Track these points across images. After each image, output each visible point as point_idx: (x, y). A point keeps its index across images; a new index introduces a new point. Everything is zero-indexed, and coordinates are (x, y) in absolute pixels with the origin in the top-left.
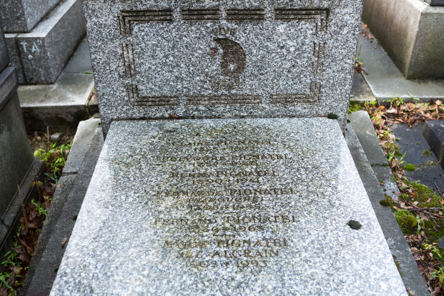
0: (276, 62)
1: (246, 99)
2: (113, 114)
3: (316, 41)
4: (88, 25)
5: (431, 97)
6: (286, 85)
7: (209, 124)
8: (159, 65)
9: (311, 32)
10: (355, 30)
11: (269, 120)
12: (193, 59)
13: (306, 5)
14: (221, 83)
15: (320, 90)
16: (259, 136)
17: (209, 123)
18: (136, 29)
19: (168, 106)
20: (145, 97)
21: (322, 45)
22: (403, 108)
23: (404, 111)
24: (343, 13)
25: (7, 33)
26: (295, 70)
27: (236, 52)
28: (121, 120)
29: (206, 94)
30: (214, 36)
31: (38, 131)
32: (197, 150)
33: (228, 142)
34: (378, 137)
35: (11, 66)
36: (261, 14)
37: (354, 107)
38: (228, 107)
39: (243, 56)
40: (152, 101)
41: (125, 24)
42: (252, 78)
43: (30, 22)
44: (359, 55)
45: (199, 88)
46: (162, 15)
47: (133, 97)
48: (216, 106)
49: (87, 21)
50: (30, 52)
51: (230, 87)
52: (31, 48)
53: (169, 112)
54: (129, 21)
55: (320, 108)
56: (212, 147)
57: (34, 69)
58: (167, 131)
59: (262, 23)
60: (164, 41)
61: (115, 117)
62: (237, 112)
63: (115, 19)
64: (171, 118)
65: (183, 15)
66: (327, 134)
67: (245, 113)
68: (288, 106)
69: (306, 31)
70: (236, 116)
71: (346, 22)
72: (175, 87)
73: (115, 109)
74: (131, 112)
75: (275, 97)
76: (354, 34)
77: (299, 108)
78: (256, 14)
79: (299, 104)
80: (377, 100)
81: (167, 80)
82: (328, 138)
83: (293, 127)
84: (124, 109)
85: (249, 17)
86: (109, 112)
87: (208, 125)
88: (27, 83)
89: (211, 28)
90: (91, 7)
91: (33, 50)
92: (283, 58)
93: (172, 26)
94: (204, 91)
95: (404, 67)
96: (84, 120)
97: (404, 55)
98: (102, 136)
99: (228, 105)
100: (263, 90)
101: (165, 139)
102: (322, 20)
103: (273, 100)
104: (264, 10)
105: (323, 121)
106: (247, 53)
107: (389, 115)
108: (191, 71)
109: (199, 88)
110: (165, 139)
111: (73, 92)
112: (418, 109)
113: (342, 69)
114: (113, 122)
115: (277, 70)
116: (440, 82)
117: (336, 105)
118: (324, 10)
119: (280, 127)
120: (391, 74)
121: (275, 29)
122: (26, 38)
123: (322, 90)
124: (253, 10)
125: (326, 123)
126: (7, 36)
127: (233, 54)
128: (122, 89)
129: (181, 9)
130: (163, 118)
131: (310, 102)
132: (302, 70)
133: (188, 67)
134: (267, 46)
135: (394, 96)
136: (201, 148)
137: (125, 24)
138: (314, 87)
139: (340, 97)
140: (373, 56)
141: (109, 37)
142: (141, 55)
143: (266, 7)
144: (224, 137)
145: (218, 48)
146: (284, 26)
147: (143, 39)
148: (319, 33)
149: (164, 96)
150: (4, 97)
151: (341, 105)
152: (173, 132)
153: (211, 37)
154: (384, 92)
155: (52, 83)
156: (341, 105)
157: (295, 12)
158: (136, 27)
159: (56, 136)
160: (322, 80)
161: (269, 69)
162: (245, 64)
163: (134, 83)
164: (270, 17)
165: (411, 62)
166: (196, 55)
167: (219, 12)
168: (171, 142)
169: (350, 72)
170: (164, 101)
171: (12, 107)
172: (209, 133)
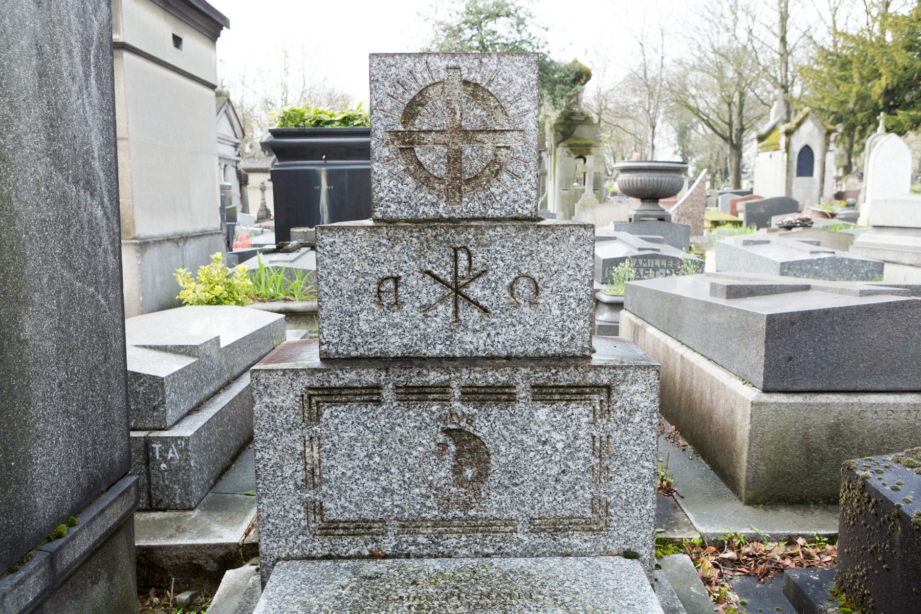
0: (536, 466)
1: (492, 525)
2: (281, 549)
3: (595, 433)
4: (257, 407)
5: (787, 532)
6: (554, 503)
7: (434, 566)
8: (357, 469)
9: (586, 419)
10: (651, 417)
11: (530, 561)
12: (410, 460)
13: (577, 380)
14: (453, 499)
15: (607, 511)
16: (513, 585)
17: (432, 565)
18: (326, 414)
19: (369, 537)
20: (333, 522)
21: (604, 439)
22: (745, 550)
23: (748, 555)
24: (631, 392)
25: (134, 429)
26: (566, 478)
27: (475, 450)
28: (293, 559)
29: (429, 516)
30: (442, 425)
31: (157, 588)
32: (413, 609)
33: (463, 595)
34: (712, 598)
35: (131, 475)
36: (511, 393)
37: (667, 549)
38: (464, 538)
39: (486, 456)
40: (344, 528)
41: (310, 407)
42: (501, 491)
43: (171, 415)
44: (666, 468)
45: (418, 507)
46: (366, 394)
47: (314, 522)
48: (445, 537)
49: (254, 402)
50: (165, 459)
51: (467, 506)
52: (168, 453)
53: (369, 547)
54: (318, 402)
55: (611, 541)
56: (436, 603)
57: (166, 486)
58: (365, 577)
59: (513, 406)
60: (367, 432)
61: (283, 555)
62: (478, 548)
63: (297, 399)
64: (373, 556)
65: (397, 393)
66: (625, 583)
67: (491, 548)
68: (559, 538)
69: (578, 419)
70: (476, 553)
71: (637, 405)
72: (381, 505)
73: (284, 540)
74: (309, 545)
75: (538, 521)
76: (651, 423)
77: (576, 540)
78: (505, 393)
79: (576, 534)
80: (701, 537)
81: (370, 494)
82: (626, 589)
83: (568, 572)
84: (299, 542)
85: (494, 397)
86: (275, 545)
87: (431, 568)
88: (152, 508)
89: (438, 414)
90: (263, 381)
91: (170, 455)
92: (547, 460)
93: (380, 410)
94: (425, 512)
95: (739, 485)
96: (234, 568)
97: (735, 467)
98: (259, 588)
99: (463, 535)
100: (518, 510)
101: (361, 590)
102: (601, 401)
103: (535, 528)
104: (515, 387)
105: (615, 563)
106: (492, 451)
107: (724, 562)
108: (406, 479)
109: (418, 507)
110: (361, 590)
111: (223, 523)
112: (770, 551)
113: (638, 477)
114: (279, 563)
115: (538, 477)
116: (798, 509)
117: (635, 536)
118: (603, 387)
119: (547, 571)
120: (719, 496)
121: (532, 415)
122: (162, 438)
123: (610, 510)
124: (500, 387)
125: (621, 565)
126: (133, 434)
127: (471, 453)
128: (298, 507)
129: (394, 384)
130: (360, 556)
131: (593, 531)
132: (577, 479)
133: (402, 473)
134: (522, 440)
135: (728, 531)
136: (419, 605)
137: (310, 407)
138: (597, 506)
139: (639, 522)
140: (687, 470)
141: (285, 426)
142: (330, 454)
143: (518, 384)
144: (457, 588)
145: (449, 443)
146: (547, 410)
147: (337, 429)
148: (599, 421)
149: (364, 520)
150: (111, 523)
151: (643, 536)
152: (374, 578)
153: (438, 427)
154: (711, 525)
155: (191, 509)
156: (643, 536)
157: (561, 390)
158: (326, 411)
159: (184, 597)
160: (609, 495)
161: (526, 477)
162: (488, 469)
163: (317, 497)
164: (525, 398)
165: (747, 477)
166: (415, 453)
167: (450, 390)
168: (369, 595)
169: (651, 482)
170: (363, 528)
171: (121, 541)
172: (433, 581)
